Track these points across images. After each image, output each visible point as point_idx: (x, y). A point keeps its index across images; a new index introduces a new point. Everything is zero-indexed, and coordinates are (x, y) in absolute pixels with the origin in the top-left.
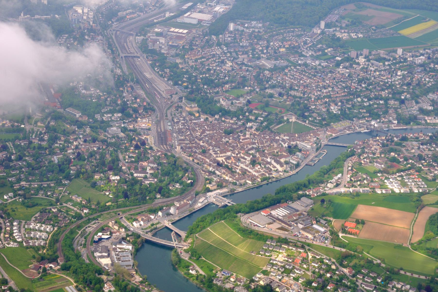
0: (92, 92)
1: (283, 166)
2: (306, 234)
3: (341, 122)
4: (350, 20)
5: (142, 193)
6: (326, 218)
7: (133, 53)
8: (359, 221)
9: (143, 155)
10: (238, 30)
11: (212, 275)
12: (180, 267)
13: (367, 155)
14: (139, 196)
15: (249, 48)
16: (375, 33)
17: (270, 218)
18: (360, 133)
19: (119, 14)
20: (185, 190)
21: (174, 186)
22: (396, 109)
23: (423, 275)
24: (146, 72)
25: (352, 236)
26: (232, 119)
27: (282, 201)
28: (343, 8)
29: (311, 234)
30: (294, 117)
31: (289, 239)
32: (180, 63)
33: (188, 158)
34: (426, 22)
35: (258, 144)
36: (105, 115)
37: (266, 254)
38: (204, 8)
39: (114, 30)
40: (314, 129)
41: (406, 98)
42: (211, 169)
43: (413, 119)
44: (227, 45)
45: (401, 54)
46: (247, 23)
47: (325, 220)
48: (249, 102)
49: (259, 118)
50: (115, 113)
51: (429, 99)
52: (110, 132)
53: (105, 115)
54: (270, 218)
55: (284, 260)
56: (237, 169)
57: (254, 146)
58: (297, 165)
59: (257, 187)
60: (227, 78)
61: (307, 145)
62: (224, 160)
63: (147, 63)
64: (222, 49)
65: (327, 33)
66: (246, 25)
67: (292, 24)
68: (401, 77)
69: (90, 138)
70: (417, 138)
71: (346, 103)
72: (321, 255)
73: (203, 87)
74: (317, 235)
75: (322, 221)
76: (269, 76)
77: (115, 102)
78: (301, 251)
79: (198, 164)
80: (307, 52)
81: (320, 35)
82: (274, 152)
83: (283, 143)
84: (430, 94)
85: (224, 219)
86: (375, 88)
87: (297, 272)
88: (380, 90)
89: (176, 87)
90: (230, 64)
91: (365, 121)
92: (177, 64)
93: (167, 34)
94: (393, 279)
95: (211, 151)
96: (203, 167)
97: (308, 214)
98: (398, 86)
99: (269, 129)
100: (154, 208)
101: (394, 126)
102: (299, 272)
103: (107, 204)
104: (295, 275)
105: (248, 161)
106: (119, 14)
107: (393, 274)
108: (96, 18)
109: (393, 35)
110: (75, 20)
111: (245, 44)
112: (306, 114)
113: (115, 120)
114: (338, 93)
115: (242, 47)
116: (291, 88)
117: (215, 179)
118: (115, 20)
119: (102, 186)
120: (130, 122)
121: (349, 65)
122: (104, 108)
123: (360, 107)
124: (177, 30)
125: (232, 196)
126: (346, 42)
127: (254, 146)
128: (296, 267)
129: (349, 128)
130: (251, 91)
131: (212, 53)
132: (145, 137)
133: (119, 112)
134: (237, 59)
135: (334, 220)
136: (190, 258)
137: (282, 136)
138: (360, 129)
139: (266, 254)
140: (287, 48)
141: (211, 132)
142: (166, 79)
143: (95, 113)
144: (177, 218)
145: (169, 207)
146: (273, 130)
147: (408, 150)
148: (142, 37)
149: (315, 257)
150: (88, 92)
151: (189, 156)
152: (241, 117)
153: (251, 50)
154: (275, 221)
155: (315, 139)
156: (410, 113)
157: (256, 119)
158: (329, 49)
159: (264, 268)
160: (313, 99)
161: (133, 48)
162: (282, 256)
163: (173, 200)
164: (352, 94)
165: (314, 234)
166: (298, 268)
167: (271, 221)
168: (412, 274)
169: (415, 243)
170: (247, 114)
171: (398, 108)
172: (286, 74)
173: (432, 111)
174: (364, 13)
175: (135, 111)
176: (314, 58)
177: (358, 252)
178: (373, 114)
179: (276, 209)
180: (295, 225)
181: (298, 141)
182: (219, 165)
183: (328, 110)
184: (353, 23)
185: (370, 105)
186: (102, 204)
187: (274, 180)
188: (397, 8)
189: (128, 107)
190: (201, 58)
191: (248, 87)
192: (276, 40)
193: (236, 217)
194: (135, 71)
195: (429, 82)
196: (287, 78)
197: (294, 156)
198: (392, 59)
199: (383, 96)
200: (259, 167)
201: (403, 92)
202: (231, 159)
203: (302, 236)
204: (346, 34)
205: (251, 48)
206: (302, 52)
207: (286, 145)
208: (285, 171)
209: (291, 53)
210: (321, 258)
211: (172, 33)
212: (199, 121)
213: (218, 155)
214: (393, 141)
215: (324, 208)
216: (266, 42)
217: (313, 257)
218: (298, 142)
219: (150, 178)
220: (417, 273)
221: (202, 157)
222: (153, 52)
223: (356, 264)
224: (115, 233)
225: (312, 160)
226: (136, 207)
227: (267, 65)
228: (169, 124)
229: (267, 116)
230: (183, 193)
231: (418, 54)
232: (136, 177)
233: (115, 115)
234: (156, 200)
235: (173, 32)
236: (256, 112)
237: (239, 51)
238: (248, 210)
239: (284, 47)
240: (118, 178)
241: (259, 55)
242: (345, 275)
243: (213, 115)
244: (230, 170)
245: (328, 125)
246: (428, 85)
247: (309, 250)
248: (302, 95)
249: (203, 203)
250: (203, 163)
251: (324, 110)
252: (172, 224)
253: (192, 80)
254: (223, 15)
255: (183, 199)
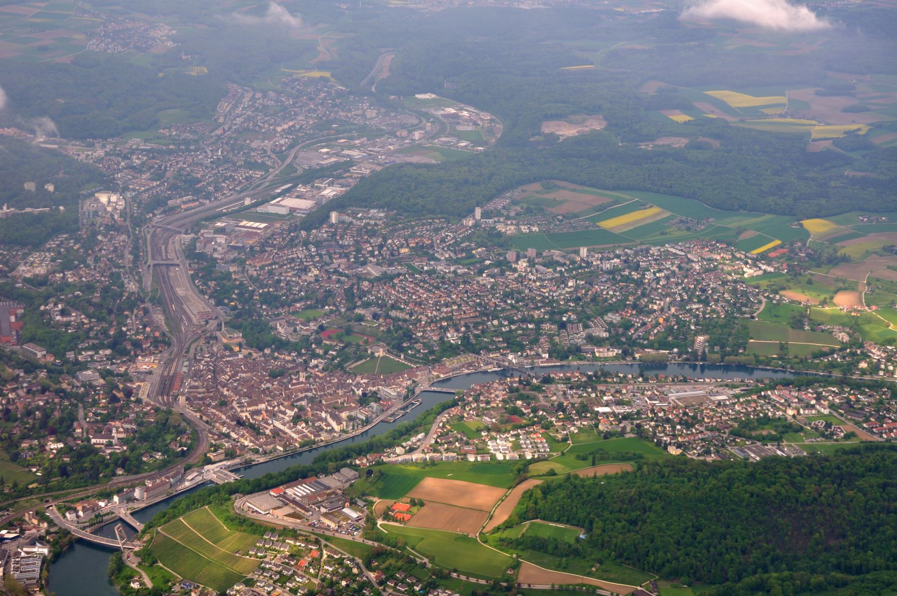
0: (72, 319)
1: (341, 423)
2: (327, 522)
3: (459, 357)
4: (525, 206)
5: (92, 468)
6: (367, 497)
7: (172, 260)
8: (414, 501)
9: (118, 411)
10: (343, 222)
11: (164, 589)
12: (117, 578)
13: (476, 405)
14: (86, 474)
15: (352, 249)
16: (560, 225)
17: (282, 501)
18: (486, 372)
19: (169, 202)
20: (169, 462)
21: (151, 456)
22: (551, 337)
23: (482, 578)
24: (180, 287)
25: (397, 524)
26: (289, 354)
27: (309, 474)
28: (520, 189)
29: (334, 521)
30: (381, 350)
31: (300, 530)
32: (234, 272)
33: (195, 414)
34: (645, 209)
35: (316, 391)
36: (83, 353)
37: (259, 554)
38: (307, 192)
39: (153, 227)
40: (412, 368)
41: (569, 321)
42: (224, 430)
43: (576, 351)
44: (318, 244)
45: (585, 256)
46: (363, 212)
47: (365, 501)
48: (322, 328)
49: (330, 352)
50: (101, 349)
51: (605, 321)
52: (80, 377)
53: (83, 353)
54: (282, 501)
55: (282, 563)
56: (267, 429)
57: (309, 394)
58: (367, 422)
59: (292, 456)
60: (302, 293)
61: (390, 392)
62: (249, 416)
63: (187, 273)
64: (308, 250)
65: (483, 226)
66: (360, 215)
67: (432, 212)
68: (572, 289)
69: (39, 388)
70: (569, 379)
71: (474, 327)
72: (342, 554)
73: (261, 307)
74: (345, 523)
75: (361, 503)
76: (366, 289)
77: (105, 332)
78: (314, 548)
79: (207, 422)
80: (442, 254)
81: (470, 228)
82: (337, 402)
83: (356, 390)
84: (610, 315)
85: (209, 503)
86: (527, 305)
87: (298, 579)
88: (534, 308)
89: (219, 308)
90: (316, 272)
91: (498, 355)
92: (230, 273)
93: (233, 230)
94: (438, 586)
95: (235, 404)
96: (214, 427)
97: (343, 493)
98: (562, 303)
99: (342, 368)
100: (108, 490)
101: (542, 362)
102: (301, 580)
103: (30, 486)
104: (294, 584)
105: (289, 416)
106: (169, 202)
107: (441, 578)
108: (128, 210)
109: (587, 227)
110: (89, 212)
111: (346, 243)
112: (405, 345)
113: (98, 360)
114: (465, 313)
115: (342, 246)
116: (393, 307)
117: (226, 445)
118: (159, 212)
119: (28, 458)
120: (124, 362)
121: (499, 273)
122: (83, 342)
123: (495, 334)
124: (250, 224)
125: (248, 470)
126: (511, 238)
127: (309, 394)
128: (300, 572)
129: (470, 365)
130: (331, 311)
131: (290, 257)
132: (137, 384)
133: (108, 347)
134: (328, 265)
135: (379, 501)
136: (140, 564)
137: (358, 379)
138: (486, 367)
139: (259, 554)
140: (413, 247)
141: (249, 374)
142: (207, 297)
143: (66, 350)
144: (143, 505)
145: (133, 487)
146: (348, 369)
147: (547, 397)
148: (192, 235)
149: (332, 557)
150: (65, 319)
151: (196, 412)
152: (303, 351)
153: (354, 251)
154: (287, 504)
155: (409, 382)
156: (571, 342)
157: (326, 353)
158: (479, 250)
159: (249, 576)
160: (423, 323)
161: (174, 252)
162: (281, 557)
163: (145, 478)
164: (486, 315)
165: (339, 522)
166: (302, 573)
167: (280, 504)
168: (468, 578)
169: (487, 533)
170: (313, 346)
171: (554, 335)
172: (394, 287)
173: (607, 339)
174: (550, 196)
175: (137, 345)
176: (450, 261)
177: (399, 548)
178: (514, 344)
179: (296, 486)
180: (317, 509)
181: (381, 385)
182: (240, 423)
183: (441, 339)
184: (529, 211)
185: (511, 331)
186: (20, 486)
187: (322, 444)
188: (605, 189)
189: (126, 340)
190: (271, 265)
191: (329, 306)
192: (398, 236)
193: (229, 499)
194: (163, 286)
195: (612, 297)
196: (393, 292)
197: (365, 407)
198: (568, 263)
199: (536, 317)
200: (304, 425)
201: (566, 311)
202: (261, 414)
203: (322, 525)
204: (512, 228)
205: (354, 249)
206: (434, 254)
207: (360, 392)
208: (343, 431)
209: (417, 255)
210: (340, 558)
211: (242, 229)
212: (236, 358)
213: (245, 409)
214: (528, 384)
215: (369, 483)
216: (380, 239)
217: (328, 556)
218: (380, 387)
219: (116, 445)
220: (474, 576)
221: (217, 413)
222: (202, 257)
223: (390, 565)
224: (30, 530)
225: (392, 415)
226: (78, 489)
227: (374, 273)
228: (186, 363)
229: (343, 348)
230: (163, 466)
231: (612, 256)
232: (95, 444)
233: (101, 352)
234: (114, 478)
235: (244, 227)
236: (328, 342)
237: (335, 253)
238: (249, 488)
239: (408, 246)
240: (61, 445)
241: (366, 258)
242: (370, 582)
243: (261, 349)
244: (255, 430)
245: (437, 361)
246: (610, 301)
247: (326, 546)
248: (407, 317)
249: (194, 482)
250: (215, 422)
251: (435, 338)
252: (132, 514)
253: (245, 297)
254: (333, 200)
255: (161, 476)
